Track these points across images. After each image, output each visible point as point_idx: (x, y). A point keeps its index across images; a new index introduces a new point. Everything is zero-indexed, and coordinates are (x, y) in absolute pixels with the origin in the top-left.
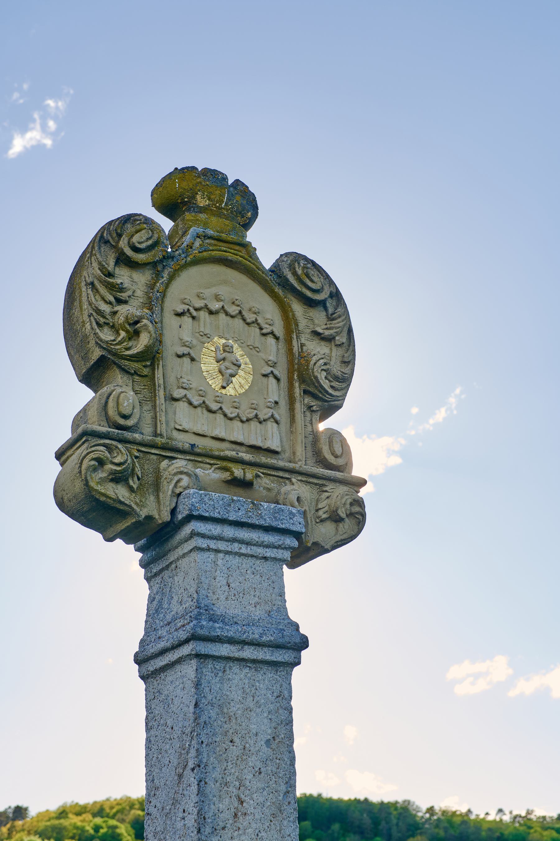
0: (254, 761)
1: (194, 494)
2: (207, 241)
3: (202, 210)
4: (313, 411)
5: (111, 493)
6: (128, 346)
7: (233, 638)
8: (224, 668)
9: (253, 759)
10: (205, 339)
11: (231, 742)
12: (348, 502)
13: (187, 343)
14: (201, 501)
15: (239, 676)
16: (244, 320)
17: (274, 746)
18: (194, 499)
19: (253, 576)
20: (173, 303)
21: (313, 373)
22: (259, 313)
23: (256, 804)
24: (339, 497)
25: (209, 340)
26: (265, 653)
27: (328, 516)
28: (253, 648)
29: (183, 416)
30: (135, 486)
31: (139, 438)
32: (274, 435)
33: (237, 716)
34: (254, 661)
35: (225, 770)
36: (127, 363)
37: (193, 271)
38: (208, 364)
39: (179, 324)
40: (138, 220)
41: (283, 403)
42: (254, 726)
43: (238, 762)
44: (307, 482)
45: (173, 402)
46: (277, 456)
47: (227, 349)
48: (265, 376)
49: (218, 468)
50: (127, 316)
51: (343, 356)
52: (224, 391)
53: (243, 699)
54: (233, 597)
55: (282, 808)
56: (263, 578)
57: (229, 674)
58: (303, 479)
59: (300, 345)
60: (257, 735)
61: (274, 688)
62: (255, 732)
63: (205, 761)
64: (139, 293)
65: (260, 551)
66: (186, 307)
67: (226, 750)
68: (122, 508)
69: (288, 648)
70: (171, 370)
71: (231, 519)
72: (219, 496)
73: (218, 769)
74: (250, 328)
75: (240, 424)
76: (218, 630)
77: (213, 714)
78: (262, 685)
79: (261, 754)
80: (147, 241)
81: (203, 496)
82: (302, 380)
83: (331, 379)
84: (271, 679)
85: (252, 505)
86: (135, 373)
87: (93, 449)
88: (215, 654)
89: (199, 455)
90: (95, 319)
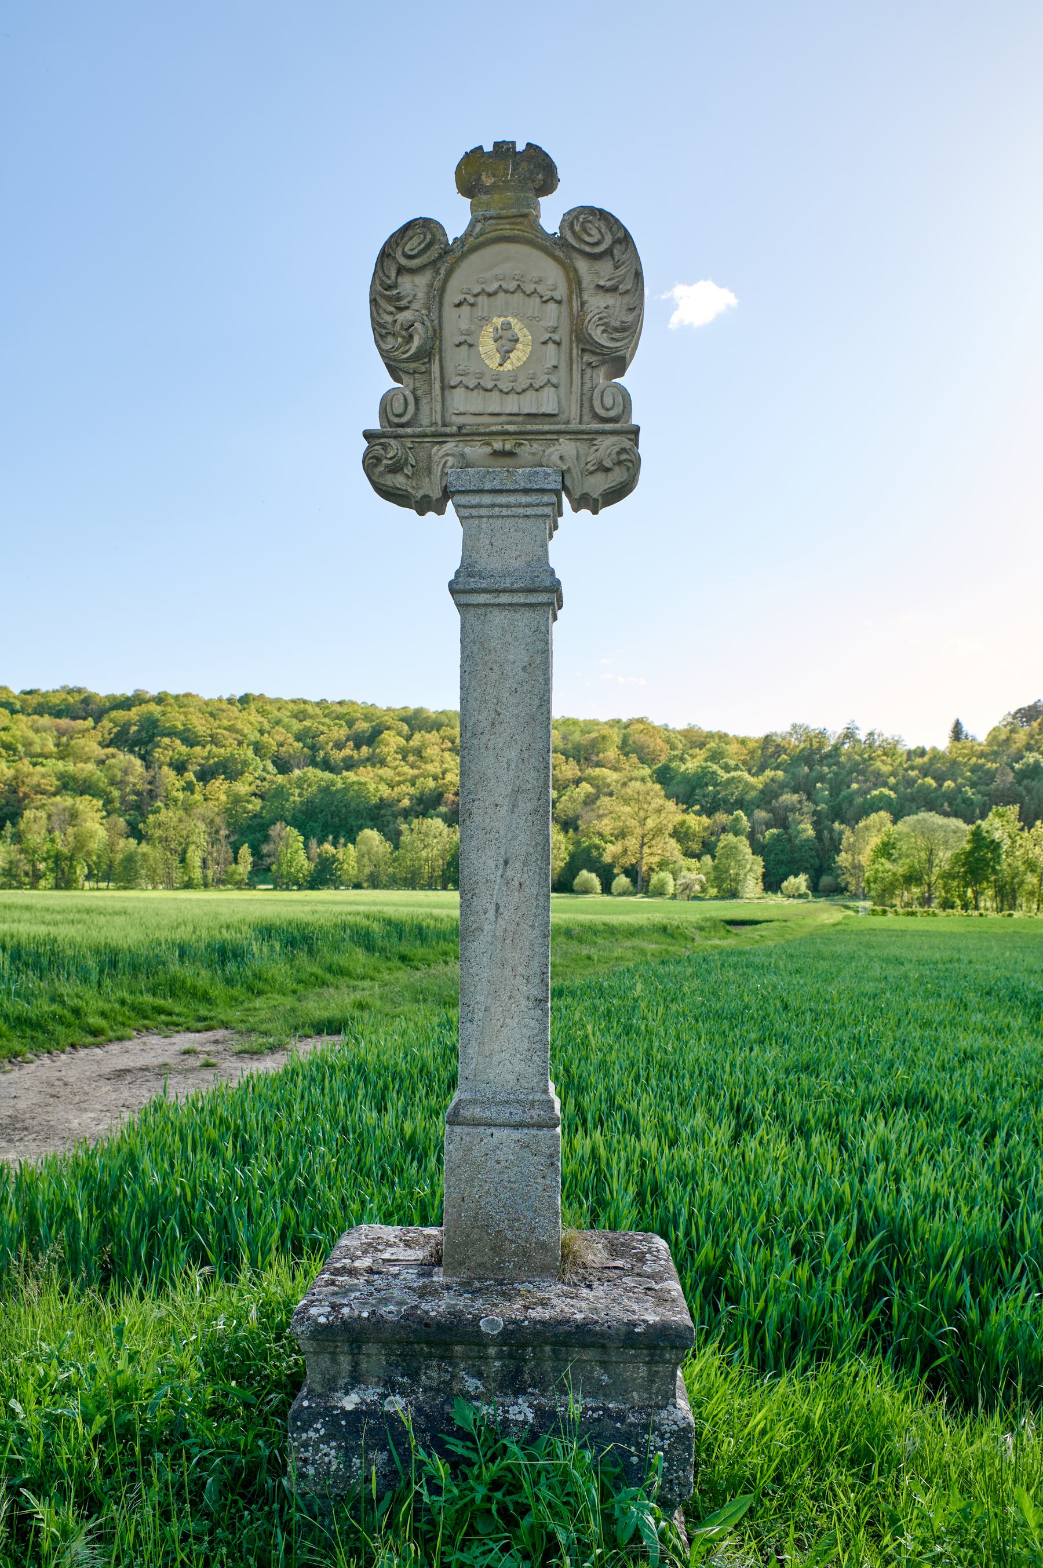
3: (494, 187)
5: (389, 483)
10: (484, 322)
14: (459, 478)
15: (498, 617)
20: (452, 296)
29: (460, 401)
34: (510, 605)
37: (474, 258)
38: (487, 346)
46: (555, 419)
47: (507, 327)
48: (545, 343)
52: (501, 369)
64: (420, 295)
65: (521, 511)
70: (455, 359)
75: (516, 396)
77: (475, 649)
82: (579, 340)
86: (415, 372)
89: (467, 435)
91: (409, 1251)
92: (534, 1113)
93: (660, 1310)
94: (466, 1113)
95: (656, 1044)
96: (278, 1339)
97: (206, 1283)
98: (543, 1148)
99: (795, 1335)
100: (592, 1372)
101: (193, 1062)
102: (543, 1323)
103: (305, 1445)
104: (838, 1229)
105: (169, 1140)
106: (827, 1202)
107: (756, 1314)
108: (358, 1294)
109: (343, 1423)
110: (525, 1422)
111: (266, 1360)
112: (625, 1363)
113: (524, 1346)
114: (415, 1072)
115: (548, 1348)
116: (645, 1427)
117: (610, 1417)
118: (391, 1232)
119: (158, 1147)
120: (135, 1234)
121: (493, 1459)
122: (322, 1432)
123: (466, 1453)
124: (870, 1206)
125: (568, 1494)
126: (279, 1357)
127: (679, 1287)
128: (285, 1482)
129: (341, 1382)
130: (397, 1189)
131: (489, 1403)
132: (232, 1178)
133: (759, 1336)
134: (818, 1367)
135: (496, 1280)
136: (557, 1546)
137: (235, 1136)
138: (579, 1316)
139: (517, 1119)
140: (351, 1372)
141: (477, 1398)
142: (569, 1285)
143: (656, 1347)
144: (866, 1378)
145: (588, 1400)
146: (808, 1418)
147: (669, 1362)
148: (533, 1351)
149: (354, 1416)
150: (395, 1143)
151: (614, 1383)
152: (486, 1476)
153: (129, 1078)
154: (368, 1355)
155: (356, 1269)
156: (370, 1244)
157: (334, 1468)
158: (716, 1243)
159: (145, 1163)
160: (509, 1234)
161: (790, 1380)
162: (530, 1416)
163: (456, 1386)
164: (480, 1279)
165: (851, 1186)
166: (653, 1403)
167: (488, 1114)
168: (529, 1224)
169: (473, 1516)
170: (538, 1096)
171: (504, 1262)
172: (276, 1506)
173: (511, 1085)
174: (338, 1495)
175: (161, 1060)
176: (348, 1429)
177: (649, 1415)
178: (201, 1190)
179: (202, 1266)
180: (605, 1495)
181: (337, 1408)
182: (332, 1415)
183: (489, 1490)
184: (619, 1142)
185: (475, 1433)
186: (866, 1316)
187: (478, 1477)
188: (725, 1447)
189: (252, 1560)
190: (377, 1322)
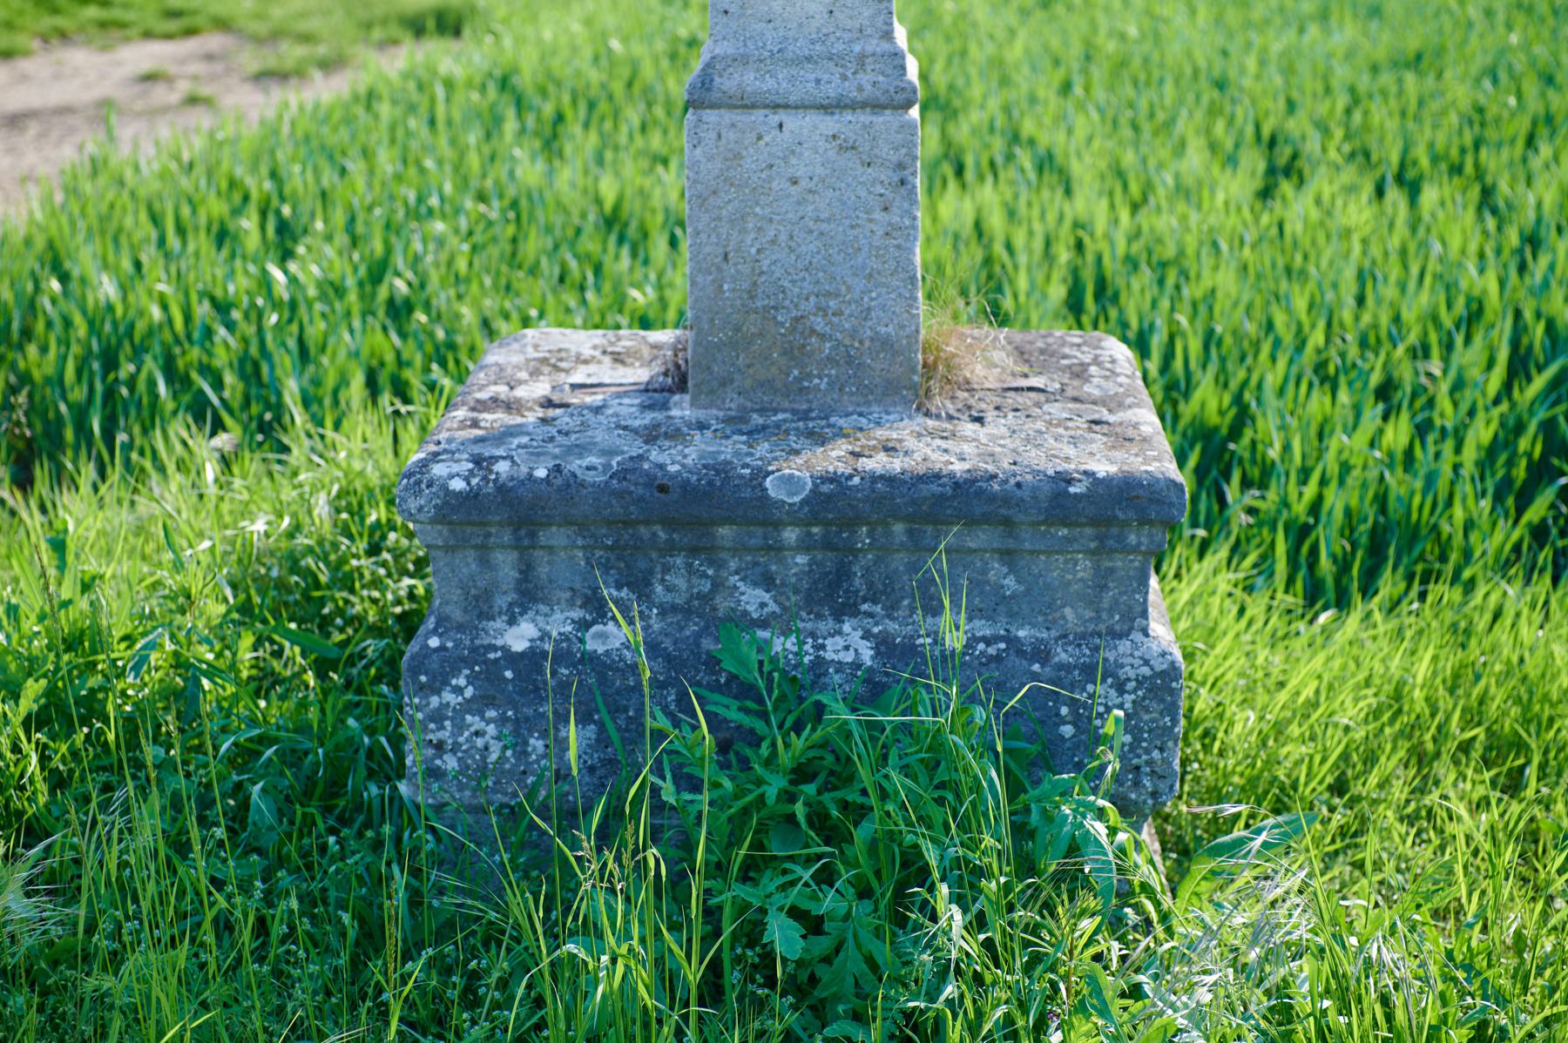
91: (621, 370)
92: (865, 79)
93: (1118, 455)
94: (727, 83)
95: (1103, 23)
96: (374, 550)
97: (225, 462)
98: (885, 151)
99: (1376, 551)
100: (985, 572)
101: (161, 95)
102: (890, 480)
103: (438, 717)
104: (1469, 357)
105: (128, 222)
106: (1449, 306)
107: (1300, 509)
108: (525, 440)
109: (508, 674)
110: (856, 665)
111: (352, 591)
112: (1049, 553)
113: (852, 523)
114: (618, 88)
115: (899, 528)
116: (1089, 672)
117: (1020, 653)
118: (584, 341)
119: (110, 232)
120: (78, 394)
121: (798, 728)
122: (469, 692)
123: (747, 721)
124: (1538, 315)
125: (941, 786)
126: (376, 583)
127: (1156, 420)
128: (403, 788)
129: (501, 602)
130: (590, 296)
131: (785, 633)
132: (266, 282)
133: (1305, 549)
134: (1422, 596)
135: (794, 412)
136: (925, 871)
137: (263, 214)
138: (958, 467)
139: (831, 91)
140: (519, 582)
141: (763, 624)
142: (938, 417)
143: (1110, 521)
144: (1518, 615)
145: (977, 623)
146: (1401, 684)
147: (1135, 550)
148: (870, 534)
149: (533, 657)
150: (583, 216)
151: (1028, 591)
152: (785, 759)
153: (33, 128)
154: (550, 549)
155: (518, 401)
156: (544, 361)
157: (493, 757)
158: (1222, 382)
159: (84, 260)
160: (819, 323)
161: (1369, 615)
162: (867, 655)
163: (723, 604)
164: (762, 411)
165: (1502, 283)
166: (1102, 627)
167: (770, 83)
168: (858, 302)
169: (761, 829)
170: (874, 45)
171: (809, 376)
172: (387, 829)
173: (815, 24)
174: (503, 806)
175: (97, 93)
176: (520, 686)
177: (1097, 649)
178: (202, 310)
179: (213, 434)
180: (1014, 789)
181: (494, 648)
182: (486, 662)
183: (791, 782)
184: (1029, 205)
185: (761, 684)
186: (1520, 511)
187: (769, 762)
188: (1238, 728)
189: (346, 918)
190: (565, 486)
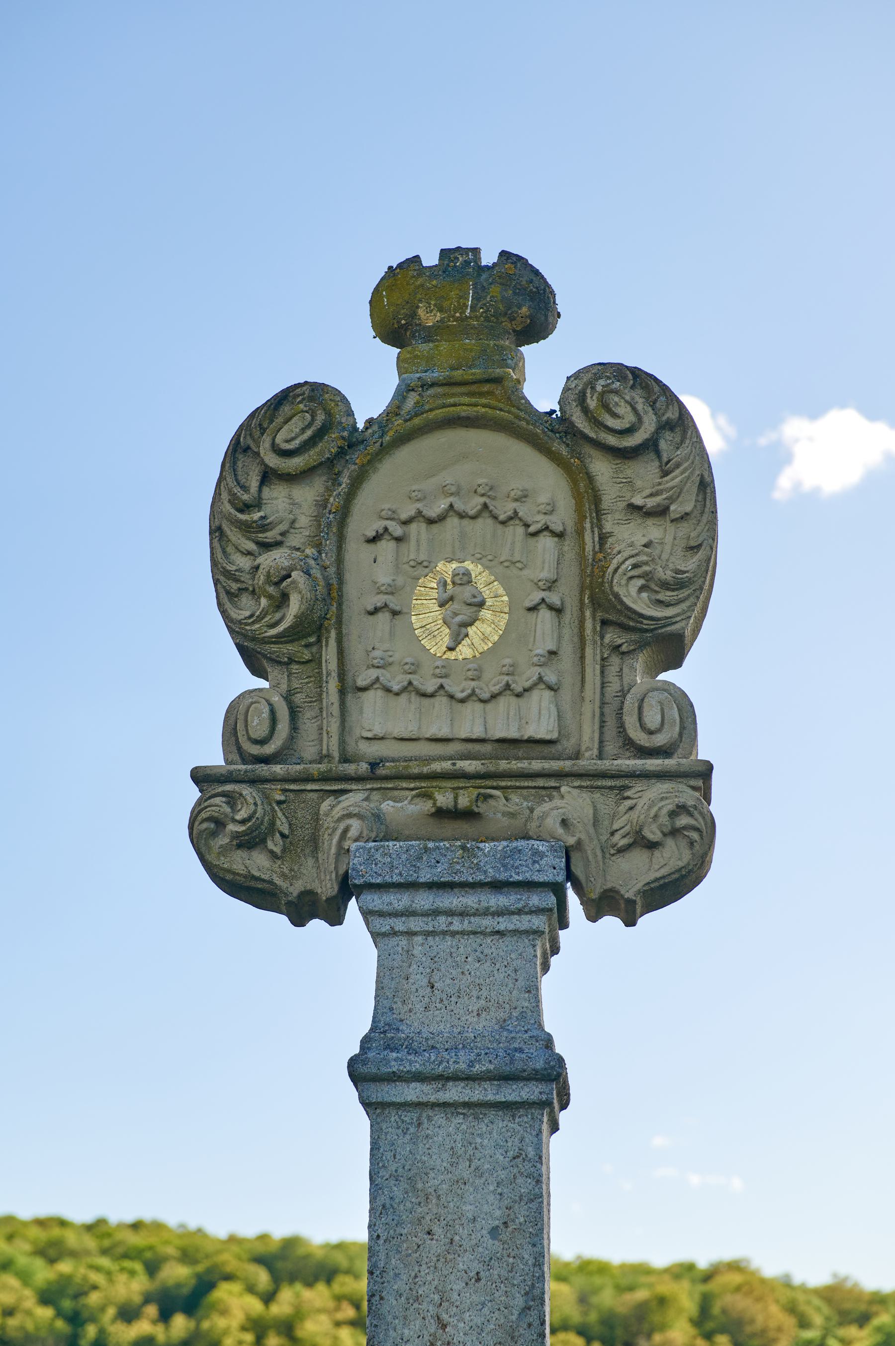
0: (466, 1262)
1: (357, 850)
2: (431, 391)
3: (439, 329)
4: (623, 653)
5: (239, 868)
6: (273, 621)
7: (420, 1073)
8: (419, 1119)
9: (465, 1259)
10: (420, 570)
11: (429, 1233)
12: (665, 811)
13: (383, 588)
15: (445, 1130)
16: (495, 518)
17: (504, 1237)
18: (357, 859)
19: (477, 965)
20: (363, 520)
21: (611, 587)
22: (526, 496)
23: (468, 1328)
24: (646, 807)
25: (427, 570)
26: (485, 1090)
27: (631, 840)
28: (462, 1084)
30: (277, 850)
31: (282, 772)
32: (543, 712)
33: (441, 1193)
34: (467, 1105)
35: (416, 1277)
36: (274, 648)
38: (426, 614)
39: (373, 556)
40: (299, 396)
41: (568, 652)
42: (469, 1207)
43: (440, 1265)
44: (592, 787)
45: (360, 694)
47: (464, 579)
48: (533, 609)
49: (418, 796)
50: (269, 572)
51: (688, 538)
52: (451, 655)
53: (452, 1165)
54: (437, 1005)
55: (516, 1334)
56: (497, 966)
57: (428, 1128)
58: (583, 784)
59: (597, 539)
60: (474, 1219)
61: (510, 1144)
62: (471, 1216)
63: (382, 1265)
64: (303, 521)
65: (488, 923)
66: (382, 524)
67: (419, 1247)
68: (260, 886)
69: (528, 1079)
70: (367, 637)
71: (422, 880)
72: (401, 847)
73: (404, 1277)
74: (508, 529)
76: (393, 1063)
77: (398, 1192)
78: (486, 1141)
79: (480, 1249)
80: (303, 433)
81: (373, 850)
82: (596, 604)
83: (657, 589)
84: (504, 1130)
85: (461, 852)
86: (291, 661)
87: (206, 804)
88: (394, 1100)
90: (224, 587)
